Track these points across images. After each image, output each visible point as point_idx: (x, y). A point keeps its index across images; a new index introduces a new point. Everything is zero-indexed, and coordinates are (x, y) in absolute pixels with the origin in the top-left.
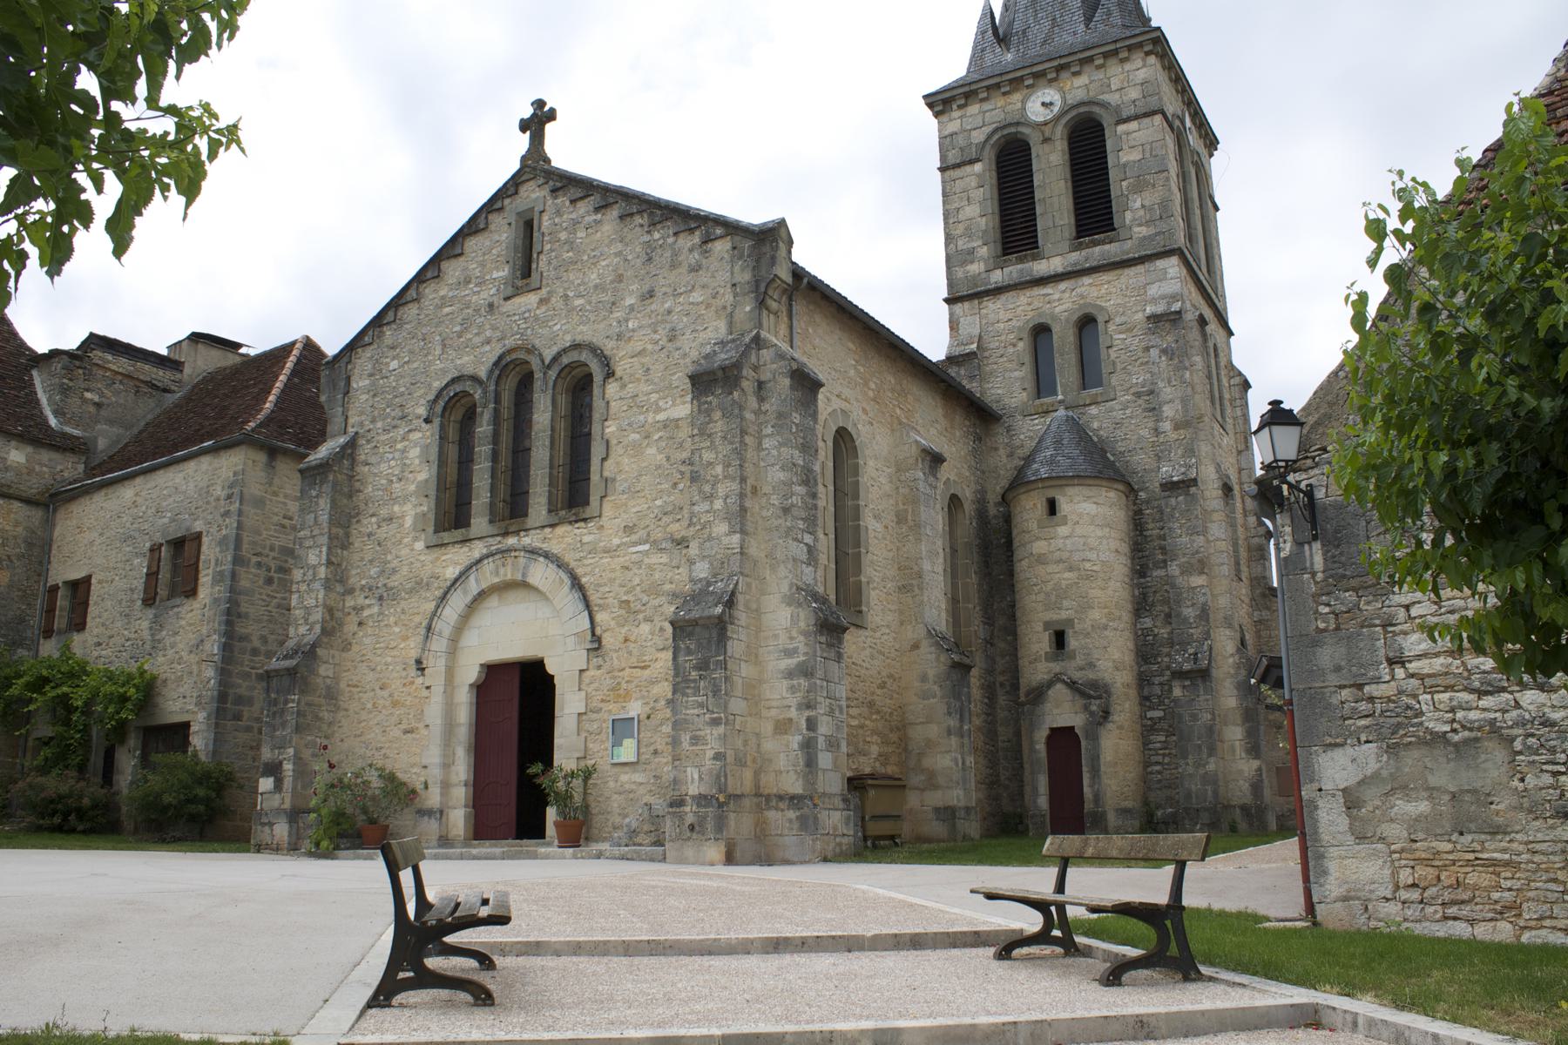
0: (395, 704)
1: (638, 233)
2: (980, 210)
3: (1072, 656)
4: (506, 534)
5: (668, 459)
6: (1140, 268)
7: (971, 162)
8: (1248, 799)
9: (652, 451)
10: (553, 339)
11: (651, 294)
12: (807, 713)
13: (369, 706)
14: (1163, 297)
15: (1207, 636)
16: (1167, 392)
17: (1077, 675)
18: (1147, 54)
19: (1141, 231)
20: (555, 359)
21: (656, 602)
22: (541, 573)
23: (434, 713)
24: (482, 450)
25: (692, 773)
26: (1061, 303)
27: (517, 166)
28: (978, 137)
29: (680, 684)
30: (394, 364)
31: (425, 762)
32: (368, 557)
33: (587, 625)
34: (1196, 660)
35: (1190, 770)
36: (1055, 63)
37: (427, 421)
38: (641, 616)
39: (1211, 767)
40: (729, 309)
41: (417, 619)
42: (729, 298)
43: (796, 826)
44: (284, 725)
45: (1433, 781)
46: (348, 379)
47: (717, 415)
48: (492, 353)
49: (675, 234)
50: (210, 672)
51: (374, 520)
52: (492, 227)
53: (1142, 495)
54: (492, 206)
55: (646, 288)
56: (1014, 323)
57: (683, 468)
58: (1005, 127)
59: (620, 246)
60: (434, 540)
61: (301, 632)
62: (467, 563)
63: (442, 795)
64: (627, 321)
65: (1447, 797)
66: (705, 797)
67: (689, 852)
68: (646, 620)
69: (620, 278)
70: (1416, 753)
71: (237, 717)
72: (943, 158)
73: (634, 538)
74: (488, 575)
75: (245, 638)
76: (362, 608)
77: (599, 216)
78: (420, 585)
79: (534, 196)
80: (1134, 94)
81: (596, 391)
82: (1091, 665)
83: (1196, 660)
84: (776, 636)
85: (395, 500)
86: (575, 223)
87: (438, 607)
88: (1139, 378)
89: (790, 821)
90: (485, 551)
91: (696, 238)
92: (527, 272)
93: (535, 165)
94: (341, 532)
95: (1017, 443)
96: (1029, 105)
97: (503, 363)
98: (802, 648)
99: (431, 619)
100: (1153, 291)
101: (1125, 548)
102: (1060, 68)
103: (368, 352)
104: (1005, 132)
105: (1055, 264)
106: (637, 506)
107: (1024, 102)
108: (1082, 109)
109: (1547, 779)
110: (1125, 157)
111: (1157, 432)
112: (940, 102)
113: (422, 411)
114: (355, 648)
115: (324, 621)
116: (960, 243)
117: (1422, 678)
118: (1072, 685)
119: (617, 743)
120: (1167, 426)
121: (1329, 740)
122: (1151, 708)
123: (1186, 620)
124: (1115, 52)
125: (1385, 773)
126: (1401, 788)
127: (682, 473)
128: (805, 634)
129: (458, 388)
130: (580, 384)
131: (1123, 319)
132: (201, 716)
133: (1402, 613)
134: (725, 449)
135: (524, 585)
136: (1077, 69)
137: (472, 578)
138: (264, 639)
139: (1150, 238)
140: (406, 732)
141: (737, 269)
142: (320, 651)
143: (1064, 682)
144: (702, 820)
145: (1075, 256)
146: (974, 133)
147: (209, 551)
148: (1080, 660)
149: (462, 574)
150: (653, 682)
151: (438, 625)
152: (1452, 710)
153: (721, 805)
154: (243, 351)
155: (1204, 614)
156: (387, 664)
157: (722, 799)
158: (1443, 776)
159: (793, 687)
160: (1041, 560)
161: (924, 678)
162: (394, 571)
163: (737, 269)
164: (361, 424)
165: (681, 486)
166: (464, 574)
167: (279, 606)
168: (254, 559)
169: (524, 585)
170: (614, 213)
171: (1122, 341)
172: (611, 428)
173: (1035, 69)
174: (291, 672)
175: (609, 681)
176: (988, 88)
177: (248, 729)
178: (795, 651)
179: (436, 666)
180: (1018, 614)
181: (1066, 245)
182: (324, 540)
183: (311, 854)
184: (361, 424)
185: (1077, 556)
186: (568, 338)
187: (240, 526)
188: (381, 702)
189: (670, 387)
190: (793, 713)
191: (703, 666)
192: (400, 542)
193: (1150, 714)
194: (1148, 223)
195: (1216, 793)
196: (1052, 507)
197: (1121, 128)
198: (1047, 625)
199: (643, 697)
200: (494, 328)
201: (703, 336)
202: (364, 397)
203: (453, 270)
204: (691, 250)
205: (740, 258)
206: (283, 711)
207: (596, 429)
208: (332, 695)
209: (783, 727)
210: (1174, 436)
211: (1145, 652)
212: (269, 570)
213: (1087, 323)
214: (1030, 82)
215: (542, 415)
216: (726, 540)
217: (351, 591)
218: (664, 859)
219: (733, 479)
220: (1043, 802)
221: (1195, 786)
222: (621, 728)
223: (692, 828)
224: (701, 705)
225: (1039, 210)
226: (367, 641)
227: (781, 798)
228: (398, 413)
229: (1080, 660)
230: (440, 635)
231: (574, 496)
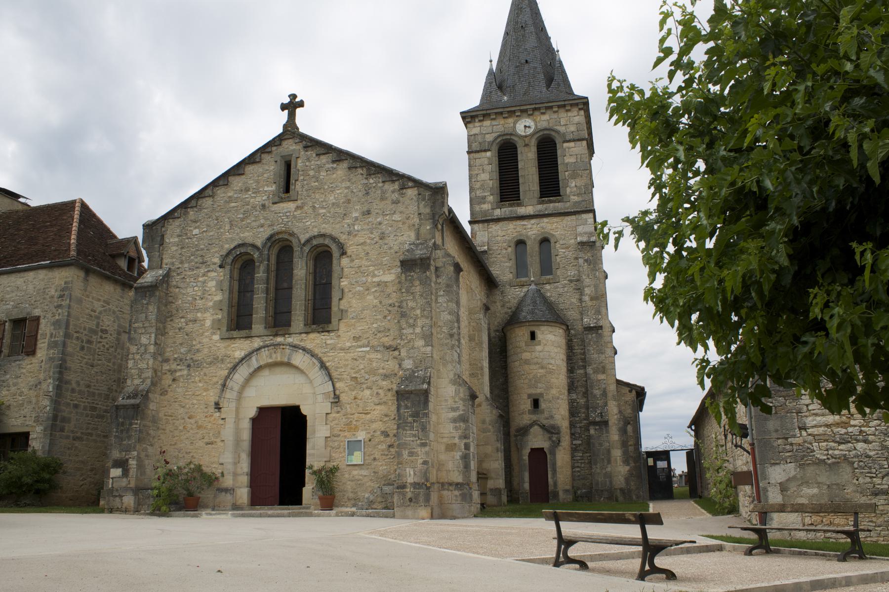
0: (199, 427)
1: (359, 178)
2: (489, 175)
3: (542, 412)
4: (276, 335)
5: (381, 302)
6: (573, 217)
7: (485, 151)
8: (623, 485)
9: (370, 297)
10: (306, 229)
11: (368, 212)
12: (465, 441)
13: (181, 428)
14: (586, 233)
15: (606, 404)
16: (587, 281)
17: (545, 422)
18: (580, 109)
19: (575, 199)
20: (308, 241)
21: (374, 379)
22: (299, 359)
23: (228, 432)
24: (259, 287)
25: (410, 471)
26: (532, 230)
27: (281, 131)
28: (490, 138)
29: (402, 424)
30: (196, 231)
31: (221, 461)
32: (179, 341)
33: (331, 389)
34: (602, 416)
35: (598, 471)
36: (533, 106)
37: (221, 267)
38: (364, 386)
39: (609, 469)
40: (417, 227)
41: (215, 379)
42: (416, 220)
43: (459, 498)
44: (129, 437)
45: (819, 480)
46: (163, 236)
47: (417, 283)
48: (265, 233)
49: (383, 182)
50: (46, 402)
51: (183, 320)
52: (264, 161)
53: (572, 332)
54: (265, 149)
55: (365, 209)
56: (506, 237)
57: (390, 308)
58: (504, 135)
59: (348, 184)
60: (227, 335)
61: (133, 383)
62: (250, 350)
63: (233, 480)
64: (354, 225)
65: (826, 487)
66: (419, 484)
67: (409, 512)
68: (368, 388)
69: (349, 201)
70: (812, 468)
71: (62, 430)
72: (469, 146)
73: (359, 343)
74: (265, 357)
75: (68, 382)
76: (175, 371)
77: (335, 165)
78: (216, 360)
79: (291, 148)
80: (573, 128)
81: (335, 262)
82: (552, 417)
83: (602, 416)
84: (446, 401)
85: (198, 310)
86: (320, 167)
87: (230, 374)
88: (572, 272)
89: (456, 496)
90: (261, 344)
91: (396, 186)
92: (287, 190)
93: (290, 130)
94: (161, 326)
95: (507, 300)
96: (517, 125)
97: (274, 239)
98: (462, 408)
99: (226, 380)
100: (580, 229)
101: (564, 357)
102: (535, 109)
103: (177, 222)
104: (504, 138)
105: (529, 210)
106: (360, 327)
107: (515, 123)
108: (545, 132)
109: (868, 480)
110: (568, 160)
111: (581, 300)
112: (468, 117)
113: (217, 260)
114: (170, 394)
115: (152, 377)
116: (478, 192)
117: (814, 436)
118: (543, 427)
119: (351, 453)
120: (586, 298)
121: (773, 462)
122: (575, 439)
123: (595, 396)
124: (564, 106)
125: (798, 476)
126: (806, 483)
127: (390, 311)
128: (463, 400)
129: (243, 250)
130: (324, 256)
131: (564, 242)
132: (39, 429)
133: (805, 408)
134: (421, 301)
135: (289, 365)
136: (544, 111)
137: (254, 359)
138: (78, 383)
139: (579, 203)
140: (207, 444)
141: (421, 206)
142: (150, 395)
143: (539, 425)
144: (417, 496)
145: (540, 207)
146: (487, 136)
147: (45, 328)
148: (546, 414)
149: (246, 356)
150: (372, 421)
151: (230, 384)
152: (827, 450)
153: (428, 488)
154: (21, 200)
155: (604, 393)
156: (193, 404)
157: (428, 485)
158: (824, 477)
159: (456, 427)
160: (527, 362)
161: (484, 422)
162: (198, 351)
163: (421, 206)
164: (173, 264)
165: (389, 318)
166: (248, 356)
167: (86, 364)
168: (76, 335)
169: (289, 365)
170: (345, 165)
171: (562, 253)
172: (344, 283)
173: (522, 108)
174: (136, 407)
175: (344, 420)
176: (496, 113)
177: (67, 437)
178: (457, 409)
179: (228, 408)
180: (511, 389)
181: (535, 201)
182: (153, 330)
183: (152, 514)
184: (173, 264)
185: (545, 362)
186: (316, 230)
187: (69, 315)
188: (189, 426)
189: (381, 264)
190: (457, 441)
191: (416, 415)
192: (202, 335)
193: (574, 442)
194: (578, 195)
195: (611, 482)
196: (533, 336)
197: (566, 145)
198: (529, 396)
199: (366, 430)
200: (266, 219)
201: (401, 239)
202: (174, 248)
203: (237, 182)
204: (393, 192)
205: (424, 199)
206: (128, 430)
207: (334, 282)
208: (155, 420)
209: (450, 448)
210: (590, 303)
211: (573, 412)
212: (82, 342)
213: (545, 241)
214: (519, 114)
215: (301, 271)
216: (423, 349)
217: (167, 361)
218: (393, 516)
219: (427, 318)
220: (527, 486)
221: (600, 479)
222: (353, 446)
223: (411, 500)
224: (414, 436)
225: (521, 181)
226: (179, 390)
227: (450, 484)
228: (199, 259)
229: (546, 414)
230: (232, 389)
231: (321, 316)
